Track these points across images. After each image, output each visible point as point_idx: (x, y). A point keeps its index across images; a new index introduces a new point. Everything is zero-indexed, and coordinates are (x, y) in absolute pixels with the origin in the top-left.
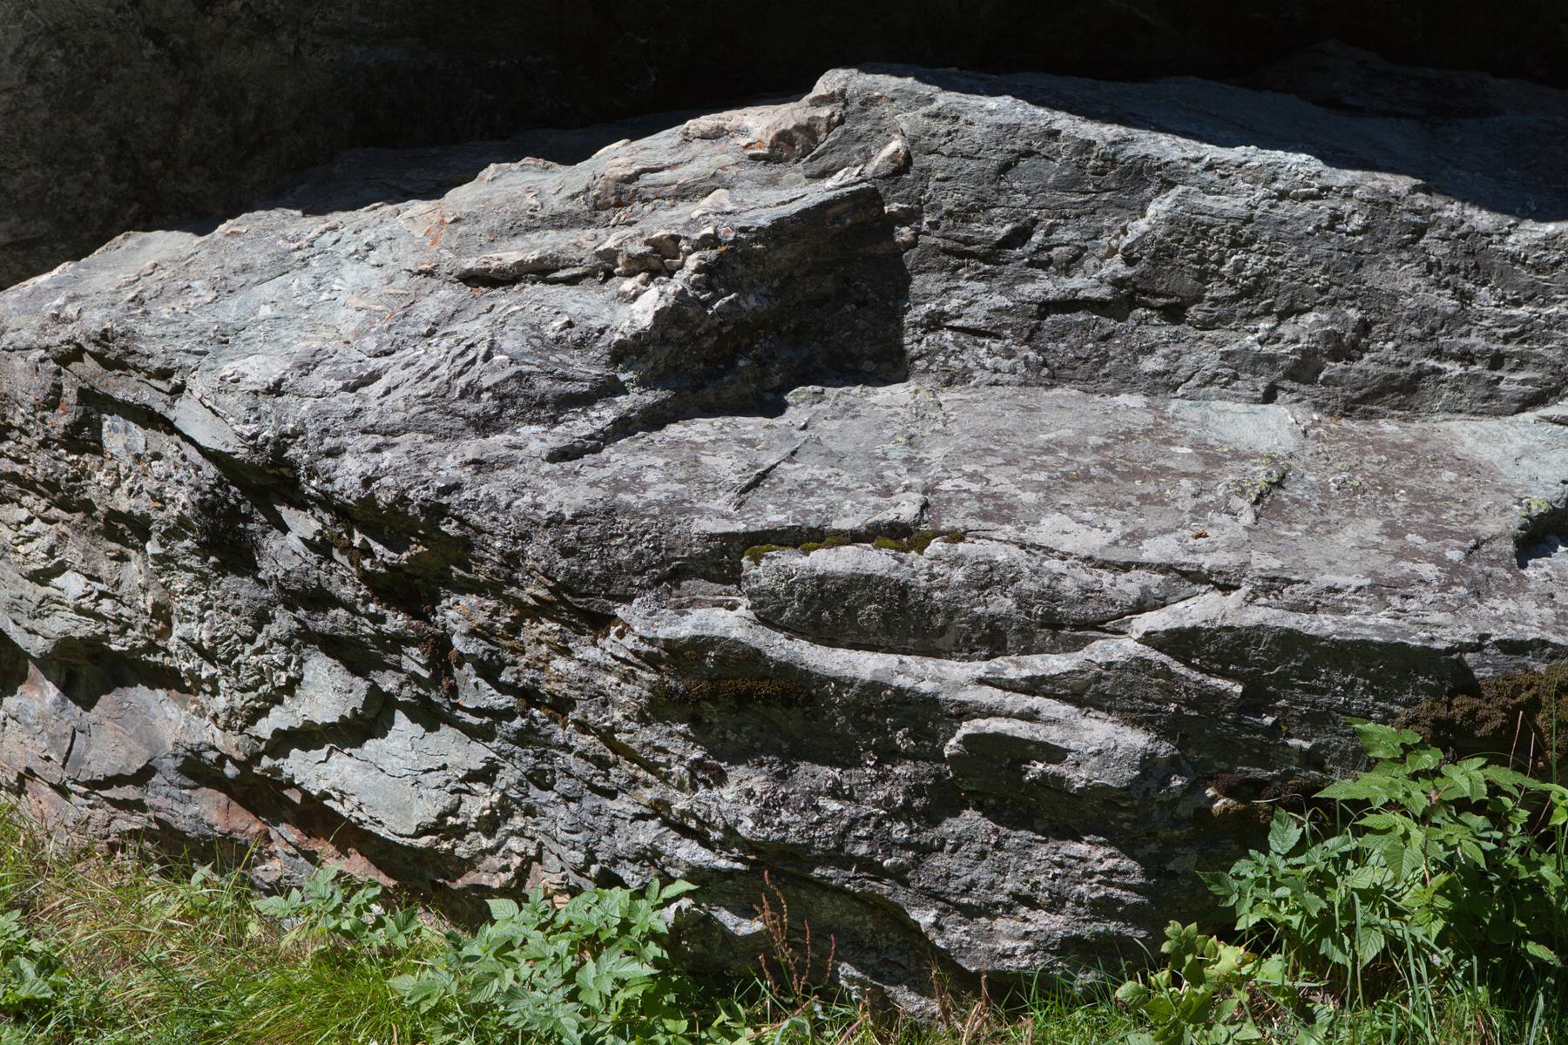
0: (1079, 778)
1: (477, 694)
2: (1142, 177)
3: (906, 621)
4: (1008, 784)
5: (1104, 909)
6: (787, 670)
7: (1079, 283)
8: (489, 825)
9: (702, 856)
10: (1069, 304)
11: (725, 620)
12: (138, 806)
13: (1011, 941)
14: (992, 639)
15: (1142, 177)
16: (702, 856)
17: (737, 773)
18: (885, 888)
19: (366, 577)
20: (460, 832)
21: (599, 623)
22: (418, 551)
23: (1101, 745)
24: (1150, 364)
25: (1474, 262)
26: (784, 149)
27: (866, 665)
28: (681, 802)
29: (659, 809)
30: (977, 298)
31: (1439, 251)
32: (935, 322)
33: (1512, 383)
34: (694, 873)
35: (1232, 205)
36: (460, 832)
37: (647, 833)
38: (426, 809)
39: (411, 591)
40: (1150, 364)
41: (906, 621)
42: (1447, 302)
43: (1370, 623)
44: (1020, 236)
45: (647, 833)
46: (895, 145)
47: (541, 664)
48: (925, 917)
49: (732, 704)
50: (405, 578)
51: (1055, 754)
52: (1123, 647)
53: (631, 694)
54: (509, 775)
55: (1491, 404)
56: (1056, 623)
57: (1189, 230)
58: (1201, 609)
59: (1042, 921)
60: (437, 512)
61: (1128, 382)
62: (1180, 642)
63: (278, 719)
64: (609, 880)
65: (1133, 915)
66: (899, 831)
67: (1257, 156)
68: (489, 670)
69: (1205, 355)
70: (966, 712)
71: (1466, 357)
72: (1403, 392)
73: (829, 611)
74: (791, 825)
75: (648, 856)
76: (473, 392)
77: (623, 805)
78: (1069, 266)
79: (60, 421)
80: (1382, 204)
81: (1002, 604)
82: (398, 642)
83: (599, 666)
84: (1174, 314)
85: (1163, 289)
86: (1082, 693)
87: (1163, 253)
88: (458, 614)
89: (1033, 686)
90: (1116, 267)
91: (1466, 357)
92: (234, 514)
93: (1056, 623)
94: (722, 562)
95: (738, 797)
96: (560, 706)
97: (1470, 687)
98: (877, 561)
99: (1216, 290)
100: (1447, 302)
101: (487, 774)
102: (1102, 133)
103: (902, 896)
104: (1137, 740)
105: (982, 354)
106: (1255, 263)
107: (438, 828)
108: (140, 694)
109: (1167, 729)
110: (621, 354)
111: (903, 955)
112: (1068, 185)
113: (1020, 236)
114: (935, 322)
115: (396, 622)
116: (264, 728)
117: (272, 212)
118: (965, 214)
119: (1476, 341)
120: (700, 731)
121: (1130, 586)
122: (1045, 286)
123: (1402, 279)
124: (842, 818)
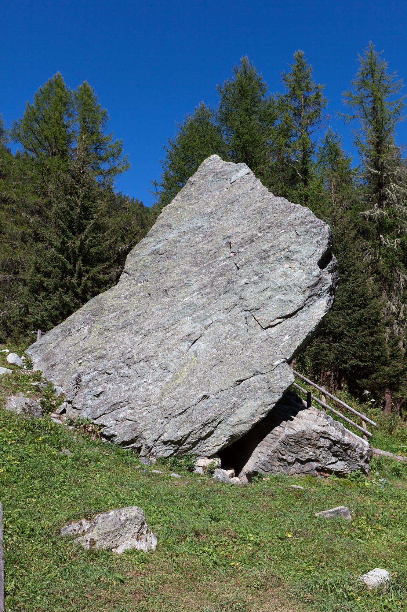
39: (345, 450)
63: (328, 463)
108: (311, 463)
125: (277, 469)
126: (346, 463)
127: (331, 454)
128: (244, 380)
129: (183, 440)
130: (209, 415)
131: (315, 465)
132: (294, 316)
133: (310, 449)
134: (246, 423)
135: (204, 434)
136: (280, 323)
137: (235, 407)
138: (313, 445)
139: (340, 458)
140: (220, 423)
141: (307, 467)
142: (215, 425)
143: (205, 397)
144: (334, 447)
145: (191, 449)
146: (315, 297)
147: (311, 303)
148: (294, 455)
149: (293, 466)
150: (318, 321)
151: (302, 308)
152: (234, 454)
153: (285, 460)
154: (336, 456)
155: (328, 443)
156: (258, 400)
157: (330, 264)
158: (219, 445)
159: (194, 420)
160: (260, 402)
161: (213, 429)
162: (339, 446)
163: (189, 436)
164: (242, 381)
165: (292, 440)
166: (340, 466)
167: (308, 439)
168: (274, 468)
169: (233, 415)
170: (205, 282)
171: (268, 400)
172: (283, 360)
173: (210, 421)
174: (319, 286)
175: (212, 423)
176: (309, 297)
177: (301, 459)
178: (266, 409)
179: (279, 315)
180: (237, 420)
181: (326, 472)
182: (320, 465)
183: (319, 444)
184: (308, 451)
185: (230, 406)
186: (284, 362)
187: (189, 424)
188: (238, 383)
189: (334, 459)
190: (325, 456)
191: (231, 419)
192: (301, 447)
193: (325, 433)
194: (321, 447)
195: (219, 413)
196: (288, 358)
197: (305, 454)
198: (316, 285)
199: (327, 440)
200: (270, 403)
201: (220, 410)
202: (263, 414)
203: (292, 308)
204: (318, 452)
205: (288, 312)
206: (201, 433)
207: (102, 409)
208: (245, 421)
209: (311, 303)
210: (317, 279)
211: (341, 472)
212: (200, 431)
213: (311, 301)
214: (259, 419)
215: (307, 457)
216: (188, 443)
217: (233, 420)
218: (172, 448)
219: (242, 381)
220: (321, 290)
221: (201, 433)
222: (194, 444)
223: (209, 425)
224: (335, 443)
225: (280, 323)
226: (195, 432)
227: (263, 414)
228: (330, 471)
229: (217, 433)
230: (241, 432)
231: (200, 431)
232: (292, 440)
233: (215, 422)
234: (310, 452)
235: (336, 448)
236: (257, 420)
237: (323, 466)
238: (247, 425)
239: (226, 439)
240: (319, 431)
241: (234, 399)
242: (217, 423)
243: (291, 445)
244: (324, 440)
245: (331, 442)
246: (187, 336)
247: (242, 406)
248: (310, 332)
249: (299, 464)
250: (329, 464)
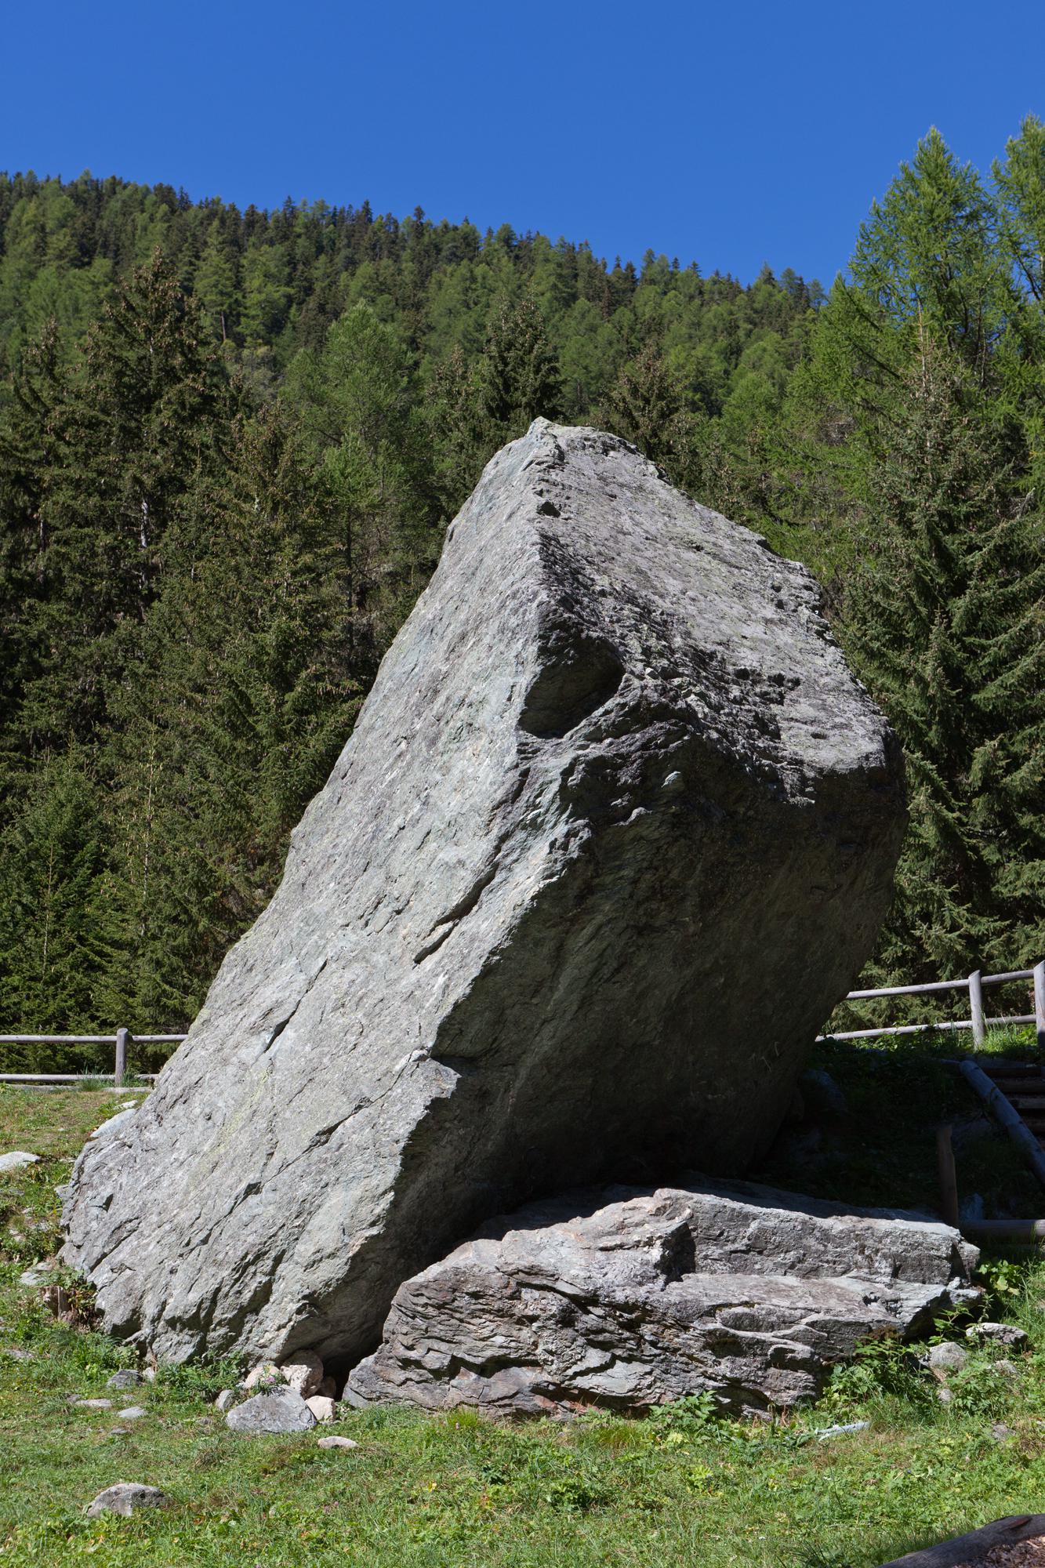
0: (799, 1357)
1: (649, 1350)
2: (746, 1218)
3: (755, 1324)
4: (782, 1360)
5: (805, 1388)
6: (734, 1335)
7: (737, 1246)
8: (649, 1387)
9: (715, 1384)
10: (736, 1252)
11: (715, 1325)
12: (510, 1405)
13: (786, 1398)
14: (772, 1327)
15: (746, 1218)
16: (715, 1384)
17: (723, 1361)
18: (758, 1388)
19: (619, 1324)
20: (640, 1390)
21: (686, 1328)
22: (634, 1315)
23: (802, 1350)
24: (757, 1267)
25: (826, 1237)
26: (659, 1212)
27: (750, 1334)
28: (710, 1371)
29: (704, 1374)
30: (715, 1251)
31: (818, 1235)
32: (706, 1257)
33: (839, 1268)
34: (714, 1388)
35: (771, 1224)
36: (640, 1390)
37: (701, 1380)
38: (631, 1385)
39: (631, 1326)
40: (757, 1267)
41: (755, 1324)
42: (822, 1248)
43: (850, 1318)
44: (722, 1234)
45: (701, 1380)
46: (688, 1211)
47: (671, 1340)
48: (768, 1394)
49: (723, 1345)
50: (627, 1326)
51: (793, 1351)
52: (802, 1327)
53: (699, 1344)
54: (657, 1372)
55: (836, 1274)
56: (787, 1322)
57: (762, 1230)
58: (814, 1317)
59: (792, 1392)
60: (645, 1303)
61: (753, 1271)
62: (812, 1324)
63: (575, 1369)
64: (689, 1394)
65: (812, 1389)
66: (760, 1373)
67: (775, 1211)
68: (654, 1344)
69: (769, 1264)
70: (772, 1344)
71: (828, 1262)
72: (814, 1271)
73: (738, 1322)
74: (737, 1374)
75: (702, 1386)
76: (635, 1276)
77: (693, 1374)
78: (734, 1241)
79: (509, 1292)
80: (804, 1223)
81: (774, 1318)
82: (628, 1339)
83: (689, 1340)
84: (760, 1253)
85: (757, 1246)
86: (793, 1338)
87: (757, 1237)
88: (647, 1330)
89: (784, 1337)
90: (745, 1241)
91: (828, 1262)
92: (573, 1311)
93: (787, 1322)
94: (711, 1312)
95: (725, 1367)
96: (675, 1351)
97: (871, 1330)
98: (746, 1310)
99: (770, 1246)
100: (822, 1248)
101: (650, 1373)
102: (737, 1205)
103: (762, 1389)
104: (808, 1348)
105: (718, 1265)
106: (778, 1239)
107: (635, 1389)
108: (514, 1370)
109: (814, 1345)
110: (656, 1266)
111: (761, 1402)
112: (731, 1220)
113: (722, 1234)
114: (706, 1257)
115: (627, 1334)
116: (570, 1372)
117: (553, 1228)
118: (708, 1229)
119: (830, 1258)
120: (714, 1353)
121: (798, 1313)
122: (730, 1247)
123: (811, 1242)
124: (1012, 1275)
125: (400, 1392)
126: (648, 1368)
127: (581, 1340)
128: (337, 1126)
129: (203, 1314)
130: (251, 1239)
131: (529, 1376)
132: (475, 908)
133: (493, 1326)
134: (332, 1255)
135: (247, 1295)
136: (446, 936)
137: (305, 1210)
138: (500, 1313)
139: (619, 1352)
140: (278, 1260)
141: (499, 1385)
142: (267, 1269)
143: (253, 1189)
144: (585, 1318)
145: (234, 1340)
146: (520, 835)
147: (514, 856)
148: (444, 1346)
149: (453, 1382)
150: (519, 912)
151: (490, 878)
152: (335, 1343)
153: (418, 1364)
154: (604, 1346)
155: (554, 1304)
156: (354, 1184)
157: (609, 704)
158: (284, 1326)
159: (221, 1257)
160: (357, 1192)
161: (265, 1279)
162: (599, 1311)
163: (214, 1301)
164: (330, 1131)
165: (423, 1300)
166: (621, 1379)
167: (475, 1296)
168: (390, 1388)
169: (305, 1235)
170: (917, 691)
171: (375, 1182)
172: (417, 1053)
173: (250, 1257)
174: (526, 795)
175: (260, 1263)
176: (504, 838)
177: (467, 1358)
178: (378, 1210)
179: (437, 914)
180: (313, 1250)
181: (574, 1399)
182: (546, 1377)
183: (519, 1309)
184: (486, 1332)
185: (295, 1208)
186: (422, 1058)
187: (212, 1270)
188: (323, 1138)
189: (595, 1357)
190: (553, 1347)
191: (300, 1247)
192: (461, 1321)
193: (532, 1271)
194: (533, 1319)
195: (272, 1231)
196: (430, 1044)
197: (481, 1344)
198: (517, 794)
199: (550, 1295)
200: (381, 1190)
201: (274, 1224)
202: (373, 1224)
203: (462, 886)
204: (526, 1334)
205: (457, 899)
206: (239, 1292)
207: (100, 1242)
208: (329, 1251)
209: (514, 856)
210: (514, 776)
211: (632, 1399)
212: (236, 1288)
213: (513, 850)
214: (362, 1241)
215: (488, 1353)
216: (219, 1324)
217: (304, 1250)
218: (187, 1338)
219: (330, 1131)
220: (536, 807)
221: (239, 1292)
222: (236, 1324)
223: (252, 1269)
224: (584, 1302)
225: (446, 936)
226: (225, 1290)
227: (373, 1224)
228: (587, 1396)
229: (278, 1288)
230: (327, 1285)
231: (236, 1288)
232: (423, 1300)
233: (267, 1257)
234: (489, 1337)
235: (591, 1319)
236: (356, 1244)
237: (557, 1379)
238: (337, 1261)
239: (295, 1306)
240: (510, 1269)
241: (306, 1187)
242: (270, 1262)
243: (425, 1317)
244: (537, 1294)
245: (565, 1301)
246: (266, 1015)
247: (319, 1206)
248: (492, 953)
249: (474, 1376)
250: (576, 1374)
